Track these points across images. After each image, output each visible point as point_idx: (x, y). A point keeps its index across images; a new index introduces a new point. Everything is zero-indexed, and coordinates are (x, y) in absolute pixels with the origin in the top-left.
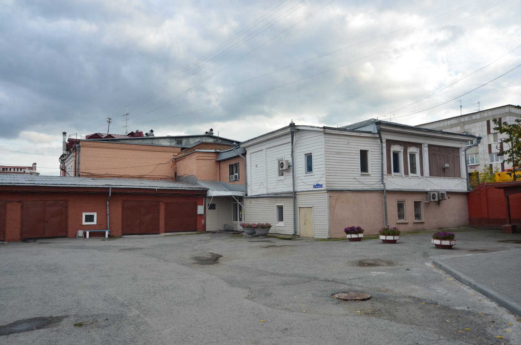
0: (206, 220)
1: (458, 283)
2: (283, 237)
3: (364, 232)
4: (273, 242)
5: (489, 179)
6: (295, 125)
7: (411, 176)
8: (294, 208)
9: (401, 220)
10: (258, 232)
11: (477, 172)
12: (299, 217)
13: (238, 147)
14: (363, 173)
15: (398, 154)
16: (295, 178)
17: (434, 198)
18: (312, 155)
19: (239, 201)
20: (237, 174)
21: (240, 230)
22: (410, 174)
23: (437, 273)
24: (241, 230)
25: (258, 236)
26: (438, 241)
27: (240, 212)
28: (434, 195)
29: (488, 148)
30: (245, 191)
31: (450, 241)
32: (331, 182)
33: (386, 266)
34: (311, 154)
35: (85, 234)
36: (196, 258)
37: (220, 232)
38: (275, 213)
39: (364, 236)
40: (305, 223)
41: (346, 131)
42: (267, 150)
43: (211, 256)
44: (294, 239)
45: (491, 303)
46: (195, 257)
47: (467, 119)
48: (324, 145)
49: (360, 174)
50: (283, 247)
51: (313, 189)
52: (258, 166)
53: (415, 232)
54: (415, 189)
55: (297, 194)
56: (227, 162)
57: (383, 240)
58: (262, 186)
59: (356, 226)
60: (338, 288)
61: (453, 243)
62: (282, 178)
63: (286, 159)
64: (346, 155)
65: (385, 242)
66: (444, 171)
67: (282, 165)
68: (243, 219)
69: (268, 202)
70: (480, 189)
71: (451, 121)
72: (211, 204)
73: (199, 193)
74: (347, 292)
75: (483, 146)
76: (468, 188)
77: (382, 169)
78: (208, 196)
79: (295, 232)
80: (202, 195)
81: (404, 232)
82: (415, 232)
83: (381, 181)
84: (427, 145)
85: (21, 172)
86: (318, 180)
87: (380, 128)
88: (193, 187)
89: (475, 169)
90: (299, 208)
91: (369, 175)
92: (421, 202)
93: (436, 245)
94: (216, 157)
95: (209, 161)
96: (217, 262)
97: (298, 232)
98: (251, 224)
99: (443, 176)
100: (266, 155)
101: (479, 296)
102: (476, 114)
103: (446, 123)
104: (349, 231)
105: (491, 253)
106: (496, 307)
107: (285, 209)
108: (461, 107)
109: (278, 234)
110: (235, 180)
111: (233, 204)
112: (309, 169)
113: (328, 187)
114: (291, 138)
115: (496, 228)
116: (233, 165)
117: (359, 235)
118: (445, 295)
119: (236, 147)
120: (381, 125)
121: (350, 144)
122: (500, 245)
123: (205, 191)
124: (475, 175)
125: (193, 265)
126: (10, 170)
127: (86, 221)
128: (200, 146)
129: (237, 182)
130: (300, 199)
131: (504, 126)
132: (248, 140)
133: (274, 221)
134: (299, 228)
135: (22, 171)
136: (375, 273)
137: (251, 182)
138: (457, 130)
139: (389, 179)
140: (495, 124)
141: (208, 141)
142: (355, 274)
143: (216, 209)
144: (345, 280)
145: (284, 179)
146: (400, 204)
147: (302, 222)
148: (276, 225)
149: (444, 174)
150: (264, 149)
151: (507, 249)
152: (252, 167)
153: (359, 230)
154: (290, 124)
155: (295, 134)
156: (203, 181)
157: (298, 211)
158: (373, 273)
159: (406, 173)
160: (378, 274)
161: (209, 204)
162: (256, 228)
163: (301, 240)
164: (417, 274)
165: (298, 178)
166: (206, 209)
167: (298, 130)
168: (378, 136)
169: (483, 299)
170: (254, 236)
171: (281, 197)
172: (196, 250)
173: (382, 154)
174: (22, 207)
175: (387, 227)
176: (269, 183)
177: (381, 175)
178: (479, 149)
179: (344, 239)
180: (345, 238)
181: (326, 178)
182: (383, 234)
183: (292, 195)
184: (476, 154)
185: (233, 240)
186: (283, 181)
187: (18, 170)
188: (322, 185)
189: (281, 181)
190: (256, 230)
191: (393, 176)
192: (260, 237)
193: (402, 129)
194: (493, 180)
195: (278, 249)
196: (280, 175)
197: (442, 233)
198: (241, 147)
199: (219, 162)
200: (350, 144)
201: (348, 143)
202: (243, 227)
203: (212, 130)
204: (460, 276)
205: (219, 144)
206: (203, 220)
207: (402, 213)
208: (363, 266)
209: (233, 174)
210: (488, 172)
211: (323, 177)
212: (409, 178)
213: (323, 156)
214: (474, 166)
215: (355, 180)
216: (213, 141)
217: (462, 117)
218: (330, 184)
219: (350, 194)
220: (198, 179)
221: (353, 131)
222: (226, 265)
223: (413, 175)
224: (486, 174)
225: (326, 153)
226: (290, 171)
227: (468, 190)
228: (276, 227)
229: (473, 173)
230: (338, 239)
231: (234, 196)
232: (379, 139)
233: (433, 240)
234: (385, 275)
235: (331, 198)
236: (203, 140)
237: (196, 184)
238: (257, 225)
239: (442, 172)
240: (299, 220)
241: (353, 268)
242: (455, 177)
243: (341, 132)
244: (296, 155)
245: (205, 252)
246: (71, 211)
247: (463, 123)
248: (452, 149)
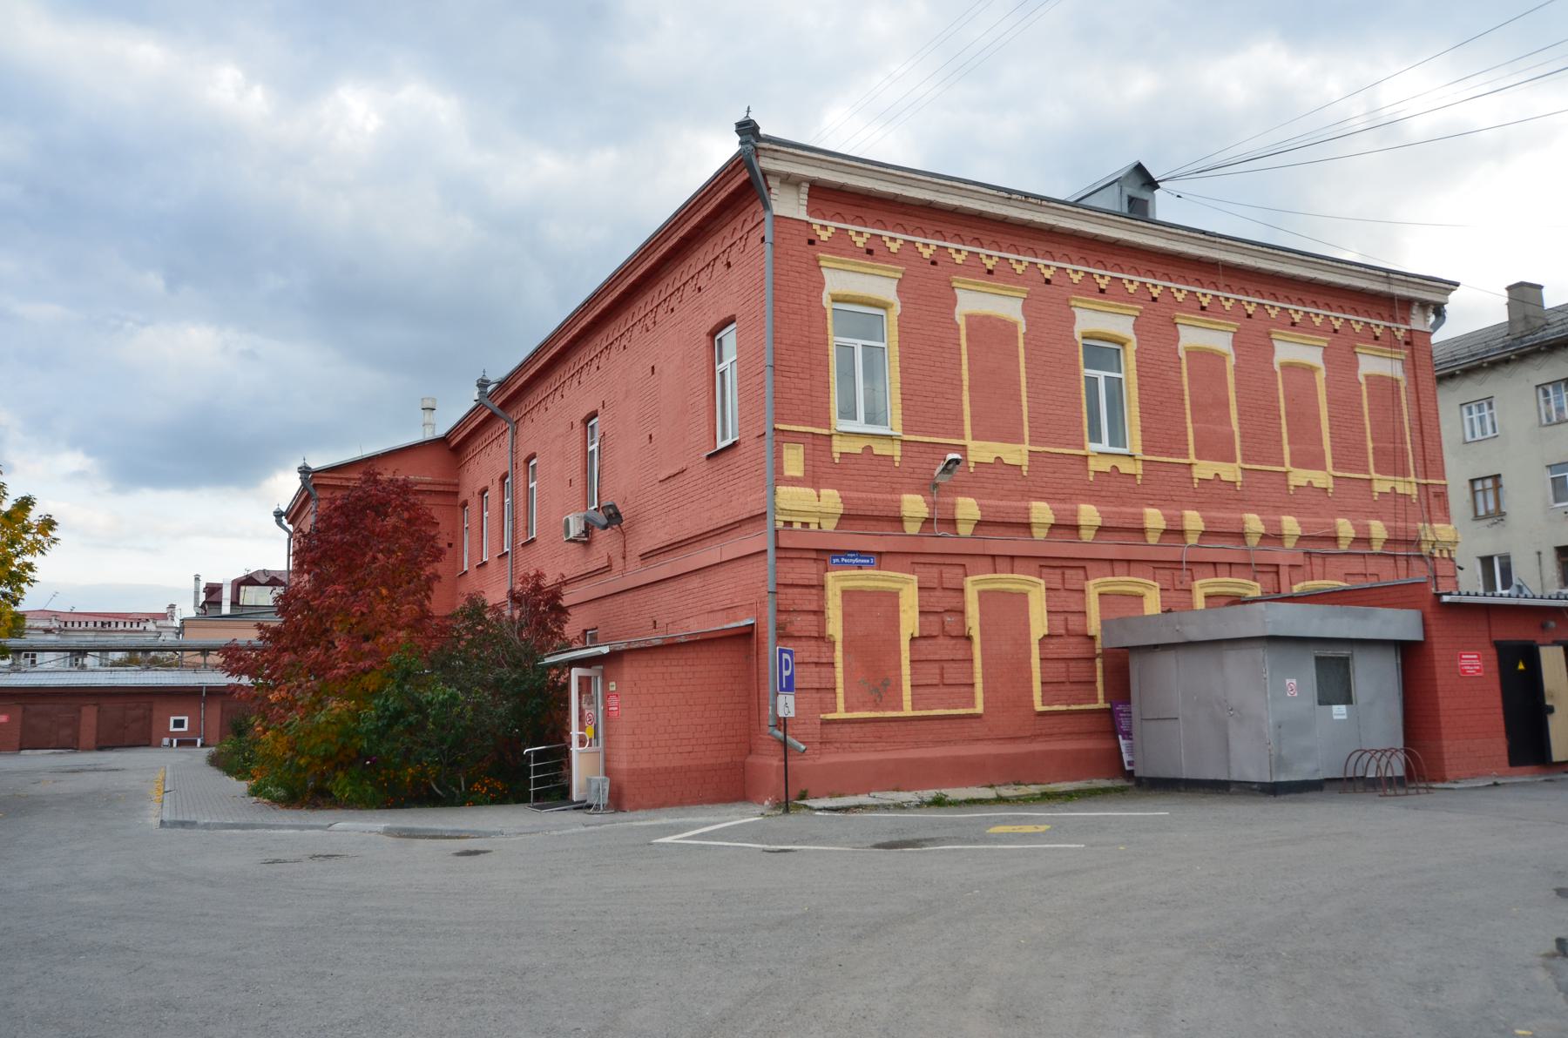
35: (171, 742)
85: (138, 629)
126: (117, 626)
127: (175, 727)
135: (141, 627)
151: (1255, 786)
174: (98, 711)
187: (131, 626)
246: (156, 715)
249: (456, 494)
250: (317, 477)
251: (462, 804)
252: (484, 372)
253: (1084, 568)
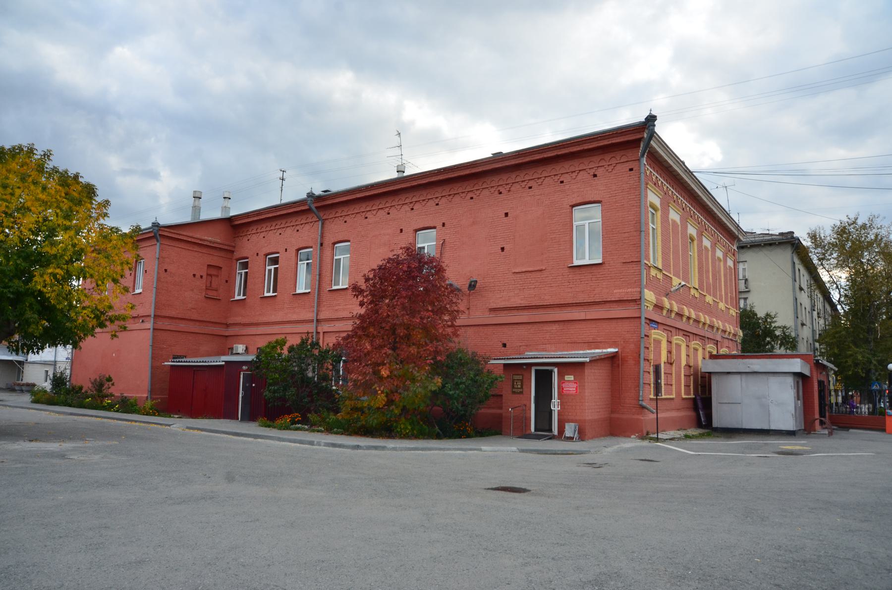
38: (43, 375)
231: (15, 361)
249: (233, 252)
250: (162, 230)
251: (460, 437)
252: (311, 189)
253: (689, 336)
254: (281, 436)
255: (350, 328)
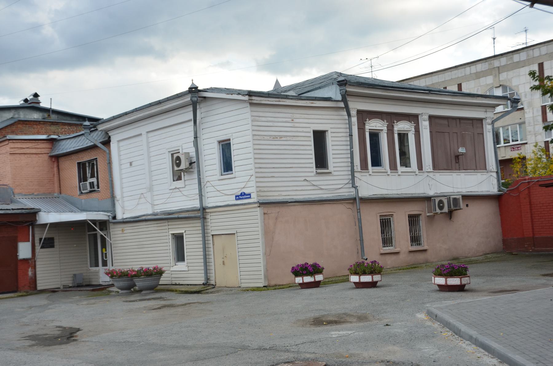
0: (37, 269)
1: (457, 339)
2: (186, 289)
3: (324, 271)
4: (169, 300)
5: (544, 168)
6: (199, 88)
7: (402, 172)
8: (202, 237)
9: (387, 248)
10: (139, 283)
11: (522, 156)
12: (212, 252)
13: (93, 129)
14: (319, 171)
15: (378, 134)
16: (202, 183)
17: (441, 208)
18: (230, 143)
19: (101, 230)
20: (94, 180)
21: (104, 284)
22: (400, 169)
23: (429, 327)
24: (107, 284)
25: (140, 291)
26: (441, 279)
27: (104, 250)
28: (441, 202)
29: (540, 113)
30: (111, 211)
31: (461, 278)
32: (265, 189)
33: (355, 322)
34: (229, 140)
36: (32, 337)
37: (66, 289)
38: (170, 246)
39: (325, 278)
40: (223, 262)
41: (288, 99)
42: (150, 135)
43: (60, 332)
44: (205, 291)
45: (491, 360)
46: (29, 336)
47: (503, 61)
48: (250, 125)
49: (315, 173)
50: (188, 305)
51: (235, 201)
52: (134, 164)
53: (412, 268)
54: (409, 194)
55: (206, 212)
56: (74, 157)
57: (355, 283)
58: (143, 200)
59: (310, 262)
60: (278, 358)
61: (465, 280)
62: (179, 184)
63: (185, 151)
64: (290, 140)
65: (360, 285)
66: (458, 159)
67: (178, 162)
68: (109, 263)
69: (156, 228)
70: (518, 188)
71: (476, 67)
72: (45, 239)
73: (20, 219)
74: (292, 362)
75: (533, 109)
76: (499, 187)
77: (352, 163)
78: (38, 223)
79: (208, 279)
80: (26, 222)
81: (393, 267)
82: (412, 267)
83: (351, 182)
84: (426, 117)
86: (242, 185)
87: (346, 91)
88: (8, 208)
89: (519, 152)
90: (213, 235)
91: (330, 173)
92: (420, 215)
93: (439, 286)
94: (51, 148)
95: (37, 156)
96: (74, 340)
97: (211, 278)
98: (126, 270)
99: (456, 169)
100: (148, 143)
101: (480, 352)
102: (519, 52)
103: (468, 70)
104: (299, 271)
105: (519, 294)
106: (496, 364)
107: (188, 240)
108: (494, 39)
109: (176, 285)
110: (91, 192)
111: (89, 235)
112: (227, 166)
113: (260, 198)
114: (192, 112)
115: (547, 253)
116: (86, 163)
117: (316, 276)
118: (433, 355)
119: (90, 129)
120: (347, 85)
121: (295, 120)
122: (543, 280)
123: (33, 214)
124: (519, 162)
125: (30, 348)
128: (14, 127)
129: (94, 195)
130: (212, 221)
131: (548, 83)
132: (113, 117)
133: (169, 261)
134: (213, 271)
136: (336, 333)
137: (122, 193)
138: (488, 83)
139: (363, 178)
140: (533, 79)
141: (30, 117)
142: (306, 337)
143: (55, 247)
144: (289, 346)
145: (184, 186)
146: (385, 221)
147: (219, 261)
148: (172, 269)
149: (457, 164)
150: (144, 133)
152: (123, 167)
153: (315, 269)
154: (190, 88)
155: (199, 105)
156: (25, 195)
157: (211, 242)
158: (333, 333)
159: (393, 167)
160: (340, 334)
161: (41, 239)
162: (135, 276)
163: (218, 292)
164: (399, 331)
165: (208, 184)
166: (36, 248)
167: (205, 97)
168: (342, 105)
169: (483, 356)
170: (132, 292)
171: (178, 218)
172: (28, 325)
173: (351, 135)
175: (361, 260)
176: (155, 193)
177: (350, 173)
178: (527, 116)
179: (292, 285)
180: (294, 285)
181: (257, 182)
182: (356, 273)
183: (198, 213)
184: (520, 124)
185: (93, 301)
186: (181, 189)
188: (250, 195)
189: (177, 190)
190: (136, 280)
191: (371, 173)
192: (143, 292)
193: (384, 91)
194: (550, 170)
195: (180, 309)
196: (175, 179)
197: (447, 266)
198: (100, 129)
199: (57, 158)
200: (295, 120)
201: (292, 120)
202: (112, 277)
203: (36, 95)
204: (460, 328)
205: (53, 123)
206: (30, 269)
207: (389, 235)
208: (319, 325)
209: (85, 180)
210: (540, 155)
211: (251, 180)
212: (399, 175)
213: (250, 144)
214: (518, 146)
215: (306, 183)
216: (40, 118)
217: (495, 58)
218: (265, 191)
219: (298, 208)
220: (17, 191)
221: (299, 97)
222: (92, 342)
223: (404, 169)
224: (537, 160)
225: (255, 138)
226: (193, 172)
227: (499, 191)
228: (173, 273)
229: (515, 158)
230: (281, 287)
231: (90, 220)
232: (345, 109)
233: (434, 278)
234: (352, 335)
235: (266, 215)
236: (19, 115)
237: (12, 202)
238: (138, 271)
239: (454, 161)
240: (212, 257)
241: (304, 329)
242: (477, 169)
243: (279, 101)
244: (202, 142)
245: (45, 326)
247: (497, 69)
248: (471, 122)
254: (127, 300)
255: (161, 278)
